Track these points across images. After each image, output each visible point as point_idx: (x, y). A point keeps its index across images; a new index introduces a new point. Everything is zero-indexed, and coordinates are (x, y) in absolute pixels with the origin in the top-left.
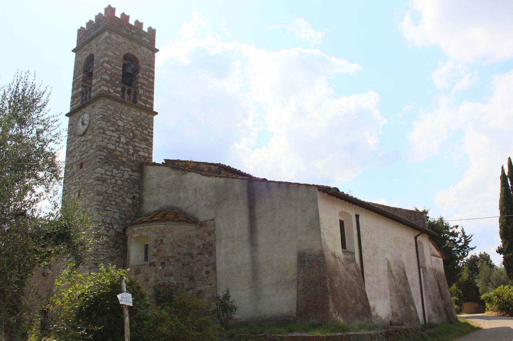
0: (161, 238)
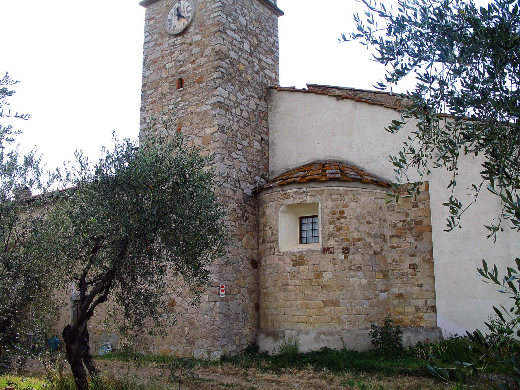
0: (340, 209)
